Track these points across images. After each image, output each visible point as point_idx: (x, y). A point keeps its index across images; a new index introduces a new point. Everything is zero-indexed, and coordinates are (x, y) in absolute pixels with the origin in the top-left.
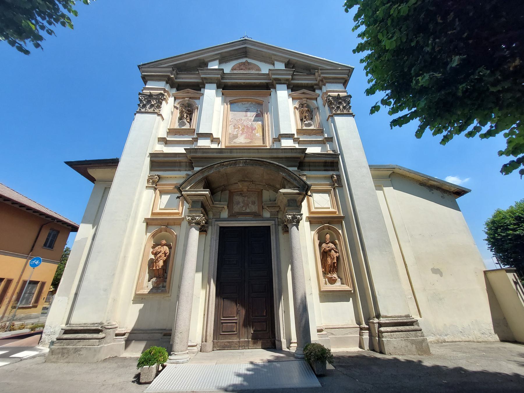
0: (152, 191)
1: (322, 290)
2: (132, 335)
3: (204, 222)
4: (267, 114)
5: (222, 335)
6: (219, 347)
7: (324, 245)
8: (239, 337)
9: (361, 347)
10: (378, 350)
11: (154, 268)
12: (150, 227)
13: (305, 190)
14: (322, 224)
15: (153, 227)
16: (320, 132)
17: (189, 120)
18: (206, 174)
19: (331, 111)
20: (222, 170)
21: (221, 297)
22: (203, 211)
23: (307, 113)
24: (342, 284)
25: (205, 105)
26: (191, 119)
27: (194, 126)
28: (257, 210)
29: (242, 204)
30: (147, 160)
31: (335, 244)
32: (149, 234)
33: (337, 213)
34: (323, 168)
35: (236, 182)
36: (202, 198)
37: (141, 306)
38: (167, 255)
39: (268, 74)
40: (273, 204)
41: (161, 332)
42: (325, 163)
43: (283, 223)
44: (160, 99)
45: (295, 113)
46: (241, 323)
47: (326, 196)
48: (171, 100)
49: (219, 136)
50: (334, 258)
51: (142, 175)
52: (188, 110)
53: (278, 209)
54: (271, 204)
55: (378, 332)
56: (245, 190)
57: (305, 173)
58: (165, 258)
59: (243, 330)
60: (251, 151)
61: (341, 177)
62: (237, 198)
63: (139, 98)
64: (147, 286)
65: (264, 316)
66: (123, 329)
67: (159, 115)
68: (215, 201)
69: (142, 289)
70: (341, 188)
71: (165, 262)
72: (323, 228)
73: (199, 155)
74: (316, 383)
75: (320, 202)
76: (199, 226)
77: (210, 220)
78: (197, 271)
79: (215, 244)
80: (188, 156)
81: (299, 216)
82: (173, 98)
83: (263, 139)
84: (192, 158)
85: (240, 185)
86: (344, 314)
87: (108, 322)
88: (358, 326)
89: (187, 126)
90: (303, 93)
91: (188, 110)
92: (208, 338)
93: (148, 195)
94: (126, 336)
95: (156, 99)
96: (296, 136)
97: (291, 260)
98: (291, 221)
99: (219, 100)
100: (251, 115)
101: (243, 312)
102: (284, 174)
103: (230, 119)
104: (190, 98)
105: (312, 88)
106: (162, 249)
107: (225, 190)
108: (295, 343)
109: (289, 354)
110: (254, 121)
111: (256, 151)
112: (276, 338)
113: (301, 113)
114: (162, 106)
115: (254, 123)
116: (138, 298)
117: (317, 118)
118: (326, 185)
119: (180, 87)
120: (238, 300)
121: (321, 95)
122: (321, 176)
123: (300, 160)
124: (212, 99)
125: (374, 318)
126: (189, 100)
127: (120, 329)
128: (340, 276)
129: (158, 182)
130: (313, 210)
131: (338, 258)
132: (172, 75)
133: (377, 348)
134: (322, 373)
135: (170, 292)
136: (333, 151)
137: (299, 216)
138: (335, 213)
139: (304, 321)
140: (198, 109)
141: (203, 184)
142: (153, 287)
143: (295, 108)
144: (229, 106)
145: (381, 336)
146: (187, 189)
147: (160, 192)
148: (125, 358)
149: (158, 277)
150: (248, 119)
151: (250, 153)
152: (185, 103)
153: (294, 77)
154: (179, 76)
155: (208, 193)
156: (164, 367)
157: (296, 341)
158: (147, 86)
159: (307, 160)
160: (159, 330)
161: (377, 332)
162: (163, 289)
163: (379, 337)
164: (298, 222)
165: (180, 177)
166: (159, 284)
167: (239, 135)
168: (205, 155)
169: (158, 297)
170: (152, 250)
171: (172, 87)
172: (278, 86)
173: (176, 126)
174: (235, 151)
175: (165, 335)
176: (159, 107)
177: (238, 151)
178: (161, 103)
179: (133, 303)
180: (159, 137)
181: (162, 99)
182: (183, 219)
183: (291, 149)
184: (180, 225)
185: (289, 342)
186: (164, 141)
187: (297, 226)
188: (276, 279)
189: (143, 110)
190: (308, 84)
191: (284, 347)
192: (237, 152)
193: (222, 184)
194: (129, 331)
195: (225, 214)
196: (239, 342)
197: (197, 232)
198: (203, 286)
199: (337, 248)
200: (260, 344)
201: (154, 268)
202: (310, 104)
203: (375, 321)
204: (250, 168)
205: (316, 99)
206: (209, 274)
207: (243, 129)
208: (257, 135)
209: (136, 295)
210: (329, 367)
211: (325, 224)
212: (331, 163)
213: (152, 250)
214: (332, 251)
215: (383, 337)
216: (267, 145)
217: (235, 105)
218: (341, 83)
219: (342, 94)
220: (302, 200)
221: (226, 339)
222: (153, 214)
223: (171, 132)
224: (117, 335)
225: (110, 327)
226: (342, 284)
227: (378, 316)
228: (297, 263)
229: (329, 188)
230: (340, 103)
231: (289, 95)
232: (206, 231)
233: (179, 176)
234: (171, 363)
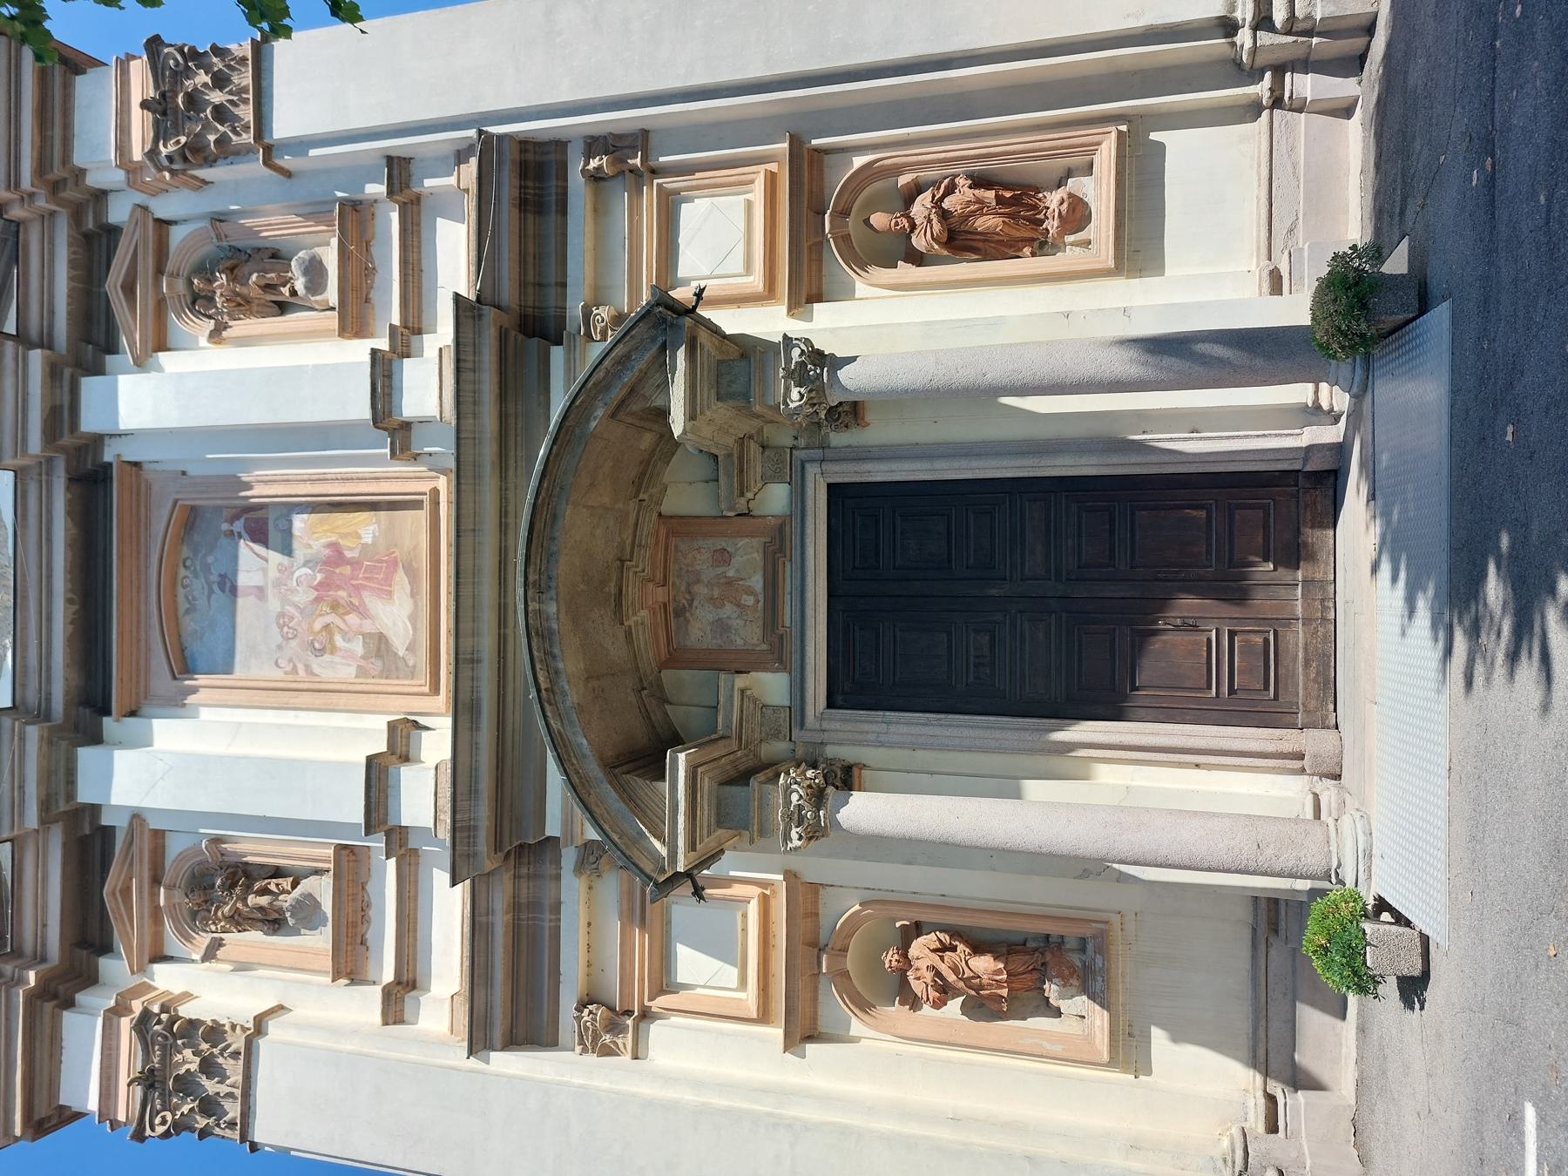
0: (656, 1029)
1: (1111, 264)
2: (1273, 1065)
3: (810, 774)
4: (248, 486)
5: (1276, 693)
6: (1323, 702)
7: (920, 242)
8: (1290, 620)
9: (1347, 112)
10: (1358, 43)
11: (1004, 992)
12: (823, 1026)
13: (670, 319)
14: (819, 246)
15: (823, 1011)
16: (354, 218)
17: (286, 883)
18: (594, 769)
19: (242, 153)
20: (572, 694)
21: (1125, 698)
22: (761, 777)
23: (244, 278)
24: (1089, 169)
25: (203, 802)
26: (278, 872)
27: (324, 852)
28: (757, 542)
29: (729, 610)
30: (506, 1063)
31: (917, 189)
32: (857, 1027)
33: (773, 167)
34: (552, 218)
35: (621, 636)
36: (706, 784)
37: (1158, 1036)
38: (945, 938)
39: (20, 475)
40: (729, 467)
41: (1263, 947)
42: (523, 204)
43: (819, 424)
44: (164, 1031)
45: (244, 341)
46: (1235, 611)
47: (691, 214)
48: (166, 978)
49: (380, 723)
50: (979, 201)
51: (578, 1081)
52: (229, 887)
53: (754, 447)
54: (729, 476)
55: (1289, 33)
56: (660, 595)
57: (575, 309)
58: (961, 947)
59: (1261, 603)
60: (467, 563)
61: (595, 132)
62: (699, 631)
63: (167, 1135)
64: (1080, 1018)
65: (1209, 518)
66: (1251, 1103)
67: (260, 1023)
68: (715, 730)
69: (1089, 1039)
70: (654, 141)
71: (978, 949)
72: (844, 241)
73: (483, 813)
74: (1439, 317)
75: (720, 243)
76: (830, 790)
77: (800, 752)
78: (1017, 795)
79: (904, 729)
80: (489, 866)
81: (796, 353)
82: (158, 968)
83: (393, 506)
84: (497, 845)
85: (640, 617)
86: (1212, 169)
87: (1220, 1164)
88: (1266, 113)
89: (322, 889)
90: (129, 289)
91: (229, 887)
92: (1287, 747)
93: (672, 1044)
94: (1276, 1088)
95: (168, 1051)
96: (383, 344)
97: (982, 396)
98: (816, 389)
99: (167, 733)
100: (254, 564)
101: (1188, 605)
102: (600, 412)
103: (279, 674)
104: (156, 881)
105: (96, 244)
106: (922, 964)
107: (661, 687)
108: (1316, 392)
109: (1355, 416)
110: (287, 550)
111: (467, 541)
112: (1297, 466)
113: (242, 305)
114: (207, 1019)
115: (300, 552)
116: (1128, 1051)
117: (274, 224)
118: (635, 211)
119: (90, 937)
120: (1136, 624)
121: (139, 198)
122: (589, 228)
123: (516, 326)
124: (157, 769)
125: (1233, 44)
126: (170, 888)
127: (1251, 1116)
128: (1055, 176)
129: (611, 1009)
130: (756, 282)
131: (979, 181)
132: (22, 981)
133: (1354, 44)
134: (1414, 293)
135: (1104, 916)
136: (461, 157)
137: (796, 353)
138: (772, 179)
139: (1219, 351)
140: (217, 840)
141: (639, 784)
142: (1085, 990)
143: (216, 335)
144: (202, 680)
145: (1307, 25)
146: (664, 851)
147: (662, 991)
148: (1360, 1084)
149: (1041, 973)
150: (278, 584)
151: (476, 572)
152: (187, 903)
153: (34, 332)
154: (28, 946)
155: (682, 757)
156: (1382, 905)
157: (1311, 386)
158: (93, 1105)
159: (508, 293)
160: (1254, 957)
161: (1290, 39)
162: (1090, 947)
163: (1309, 33)
164: (818, 357)
165: (590, 904)
166: (1071, 966)
167: (368, 627)
168: (486, 784)
169: (1123, 966)
170: (927, 1009)
171: (90, 979)
172: (90, 422)
173: (320, 941)
174: (466, 643)
175: (1274, 928)
176: (215, 1033)
177: (466, 626)
178: (193, 1024)
179: (1149, 1072)
180: (378, 1019)
181: (172, 1021)
182: (790, 876)
183: (458, 370)
184: (815, 888)
185: (1315, 413)
186: (399, 999)
187: (837, 363)
188: (1059, 461)
189: (233, 1110)
190: (72, 264)
191: (1331, 434)
192: (475, 633)
193: (632, 698)
194: (1259, 1078)
195: (772, 686)
196: (1307, 621)
197: (858, 799)
198: (1080, 774)
199: (935, 184)
200: (1318, 533)
201: (1004, 992)
202: (195, 257)
203: (1248, 44)
204: (565, 568)
205: (163, 224)
206: (1031, 751)
207: (335, 606)
208: (368, 539)
209: (1112, 1063)
210: (1397, 263)
211: (825, 230)
212: (529, 181)
213: (927, 1009)
214: (946, 204)
215: (1309, 17)
216: (425, 487)
217: (195, 648)
218: (68, 89)
219: (141, 83)
220: (715, 330)
221: (1294, 675)
222: (764, 1017)
223: (349, 963)
224: (1272, 1128)
225: (1239, 1154)
226: (1089, 169)
227: (1228, 27)
228: (996, 373)
229: (649, 198)
230: (193, 100)
231: (140, 364)
232: (848, 769)
233: (582, 909)
234: (1370, 877)
